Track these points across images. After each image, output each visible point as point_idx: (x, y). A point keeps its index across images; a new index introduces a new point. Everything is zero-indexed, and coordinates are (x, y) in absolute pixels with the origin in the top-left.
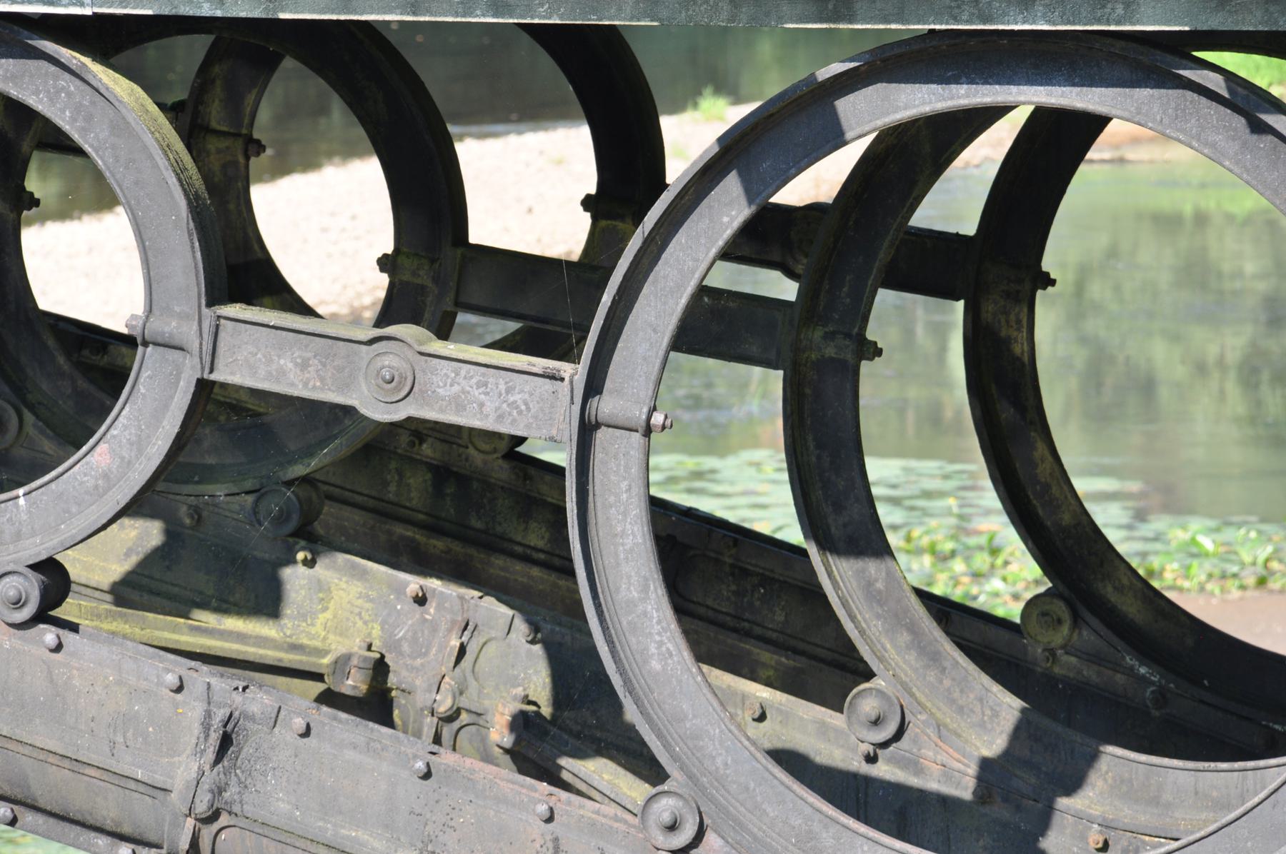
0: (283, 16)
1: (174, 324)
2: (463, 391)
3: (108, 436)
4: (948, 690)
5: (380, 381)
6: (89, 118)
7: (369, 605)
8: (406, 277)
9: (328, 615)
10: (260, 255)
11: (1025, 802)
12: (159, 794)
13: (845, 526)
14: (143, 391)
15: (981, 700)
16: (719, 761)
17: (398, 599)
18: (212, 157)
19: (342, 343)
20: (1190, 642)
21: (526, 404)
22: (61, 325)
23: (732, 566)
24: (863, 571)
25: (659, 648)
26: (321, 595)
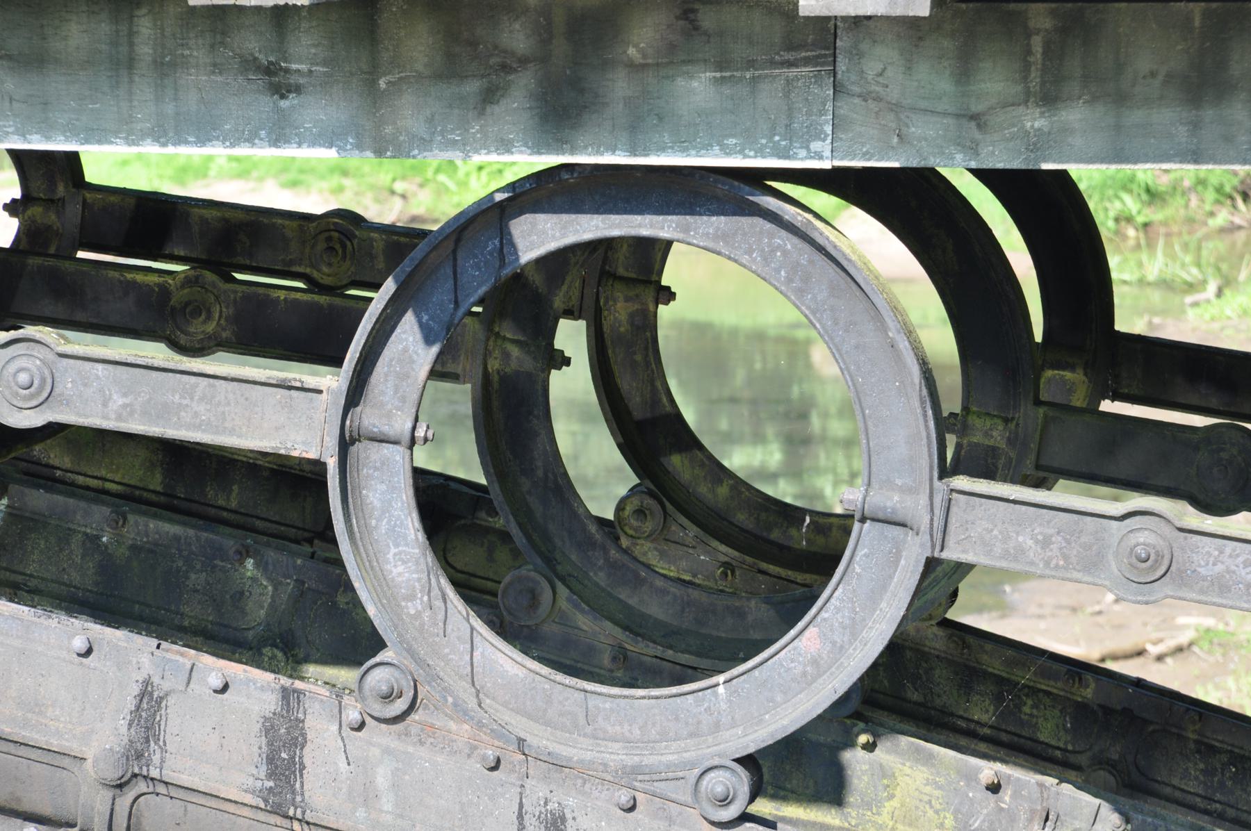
0: (1046, 166)
1: (896, 498)
2: (1228, 571)
3: (819, 619)
5: (1134, 560)
6: (806, 279)
7: (937, 793)
8: (977, 438)
9: (895, 803)
10: (669, 409)
14: (858, 570)
17: (968, 785)
18: (619, 305)
19: (1089, 519)
22: (452, 485)
23: (1196, 742)
26: (885, 781)
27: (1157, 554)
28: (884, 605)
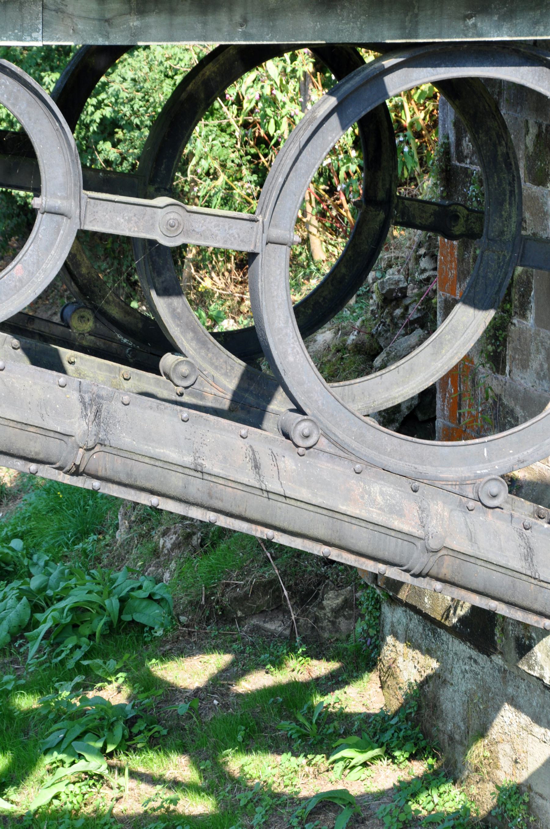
4: (211, 358)
5: (169, 227)
6: (16, 99)
11: (252, 409)
12: (65, 438)
13: (163, 282)
14: (40, 236)
15: (226, 362)
16: (320, 402)
19: (148, 208)
20: (140, 325)
21: (238, 234)
24: (171, 304)
25: (292, 350)
27: (179, 223)
28: (53, 252)
